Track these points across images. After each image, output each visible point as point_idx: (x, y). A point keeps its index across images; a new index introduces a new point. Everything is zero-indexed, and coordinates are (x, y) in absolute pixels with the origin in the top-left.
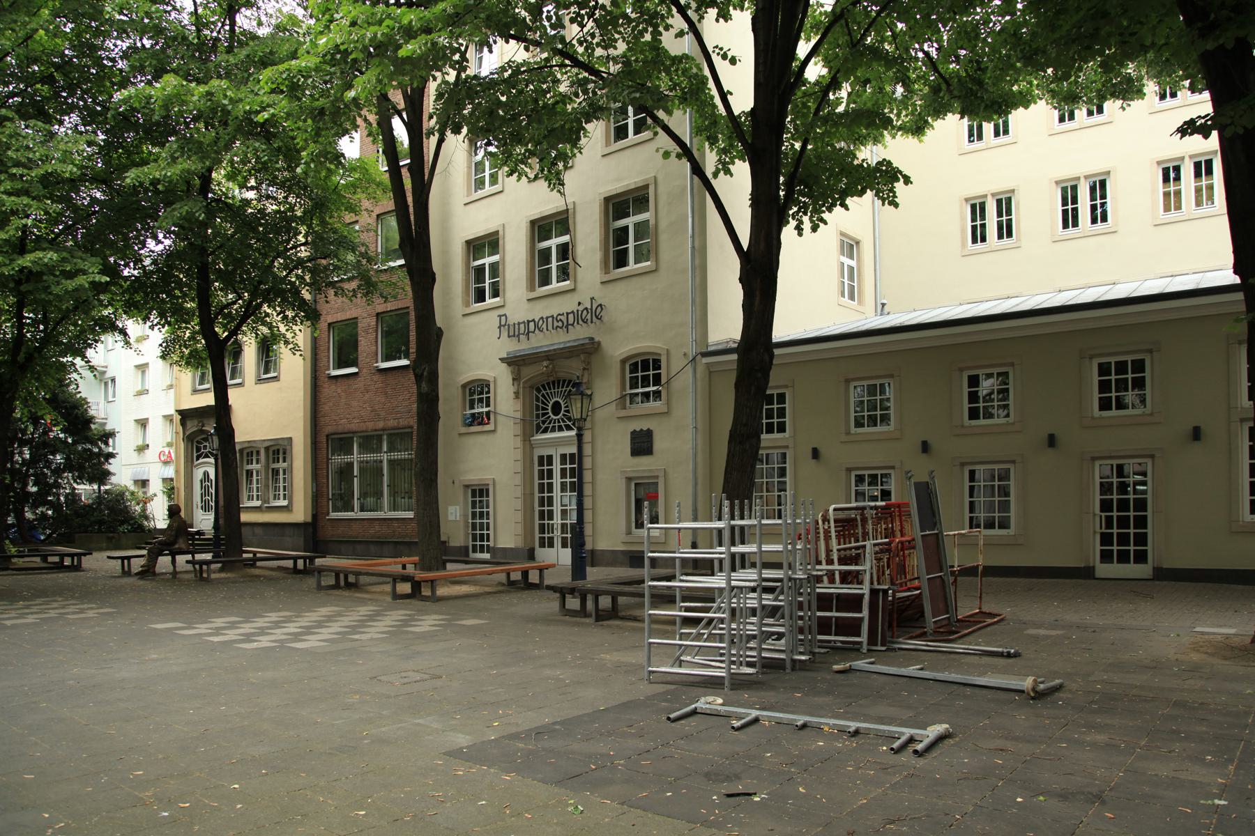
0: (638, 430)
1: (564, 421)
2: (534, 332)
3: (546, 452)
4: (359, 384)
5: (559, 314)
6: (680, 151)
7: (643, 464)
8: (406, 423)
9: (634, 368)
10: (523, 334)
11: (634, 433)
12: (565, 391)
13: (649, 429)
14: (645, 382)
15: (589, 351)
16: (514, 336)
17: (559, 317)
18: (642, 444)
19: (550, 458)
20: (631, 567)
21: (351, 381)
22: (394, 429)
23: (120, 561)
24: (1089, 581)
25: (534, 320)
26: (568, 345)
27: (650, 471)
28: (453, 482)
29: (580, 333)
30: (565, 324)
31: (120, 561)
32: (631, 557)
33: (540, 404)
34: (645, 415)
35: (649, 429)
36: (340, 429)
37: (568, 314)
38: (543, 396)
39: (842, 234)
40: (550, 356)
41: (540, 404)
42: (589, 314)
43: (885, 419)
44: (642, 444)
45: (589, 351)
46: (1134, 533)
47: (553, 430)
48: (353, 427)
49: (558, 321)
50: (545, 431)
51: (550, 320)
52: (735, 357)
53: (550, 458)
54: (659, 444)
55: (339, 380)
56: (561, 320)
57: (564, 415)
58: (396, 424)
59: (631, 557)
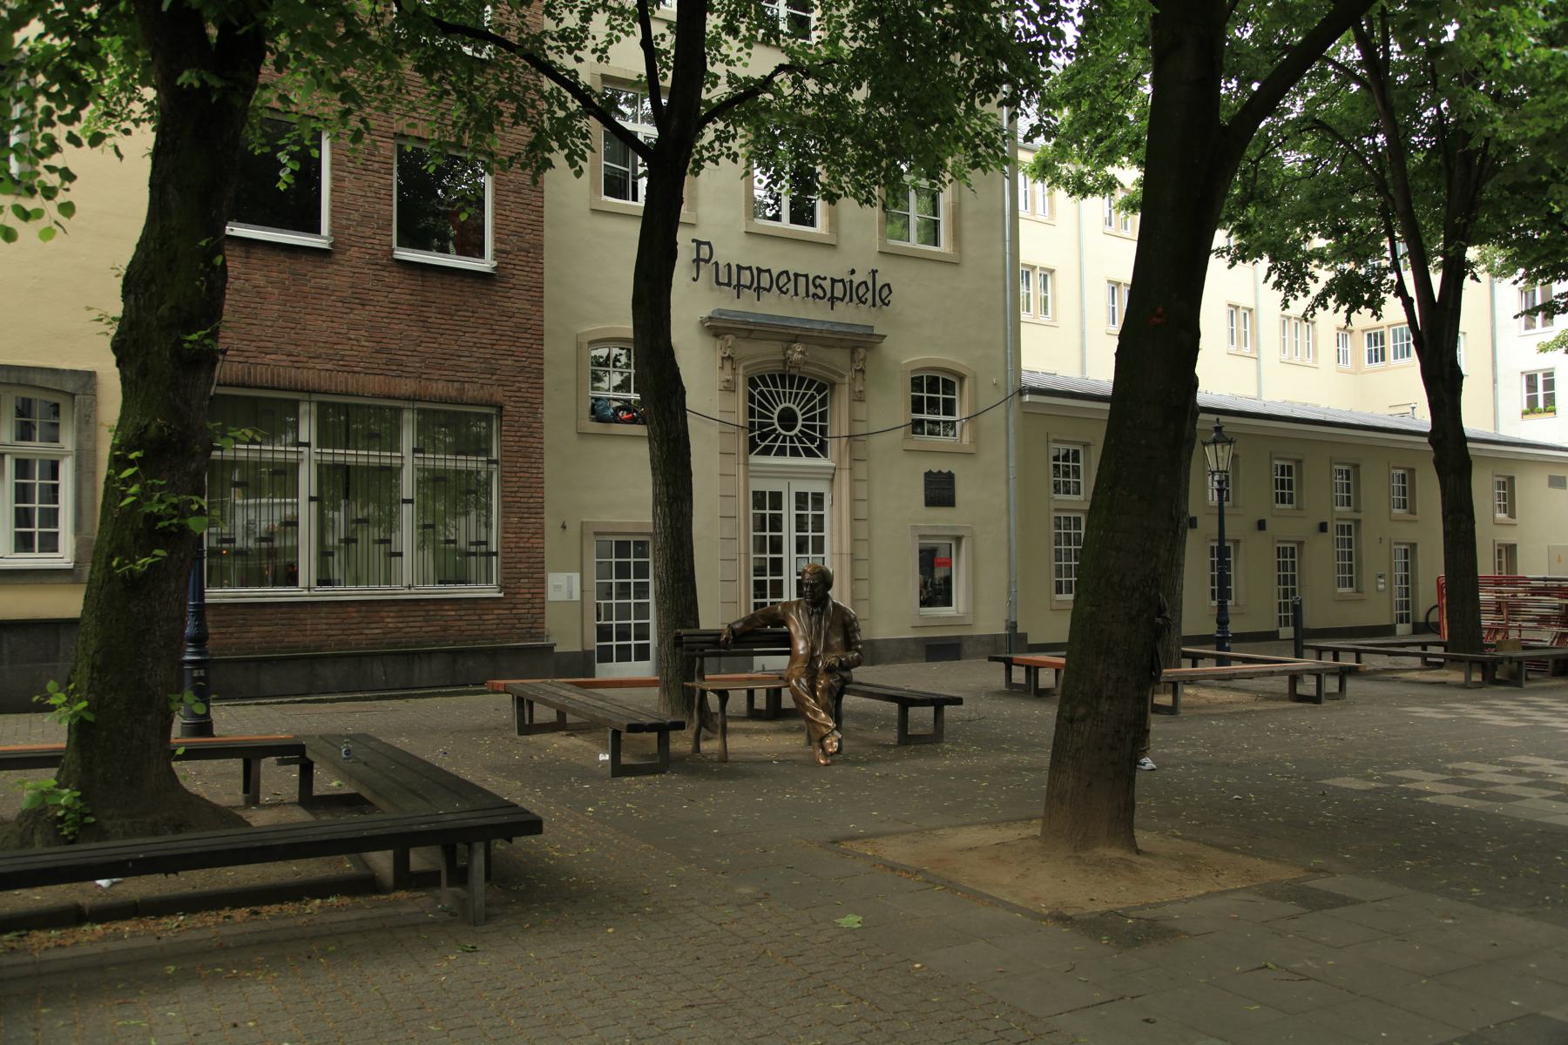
0: (935, 471)
1: (801, 442)
2: (769, 290)
3: (769, 486)
4: (337, 278)
5: (819, 277)
6: (708, 14)
7: (941, 517)
8: (483, 394)
9: (917, 383)
10: (749, 288)
11: (929, 475)
12: (804, 395)
13: (950, 472)
14: (933, 404)
15: (861, 343)
16: (729, 284)
17: (818, 281)
18: (940, 491)
19: (776, 499)
20: (927, 661)
21: (304, 265)
22: (440, 402)
23: (236, 765)
24: (1272, 643)
25: (806, 276)
26: (837, 328)
27: (953, 528)
28: (564, 527)
29: (848, 314)
30: (829, 295)
31: (236, 765)
32: (928, 646)
33: (756, 407)
34: (938, 451)
35: (950, 472)
36: (262, 374)
37: (833, 281)
38: (762, 393)
39: (1109, 281)
40: (787, 333)
41: (756, 407)
42: (870, 292)
43: (823, 448)
44: (940, 491)
45: (861, 343)
46: (40, 533)
47: (781, 452)
48: (309, 377)
49: (816, 287)
50: (766, 451)
51: (802, 280)
52: (1107, 406)
53: (776, 499)
54: (961, 493)
55: (260, 253)
56: (820, 286)
57: (780, 434)
58: (453, 394)
59: (928, 646)
